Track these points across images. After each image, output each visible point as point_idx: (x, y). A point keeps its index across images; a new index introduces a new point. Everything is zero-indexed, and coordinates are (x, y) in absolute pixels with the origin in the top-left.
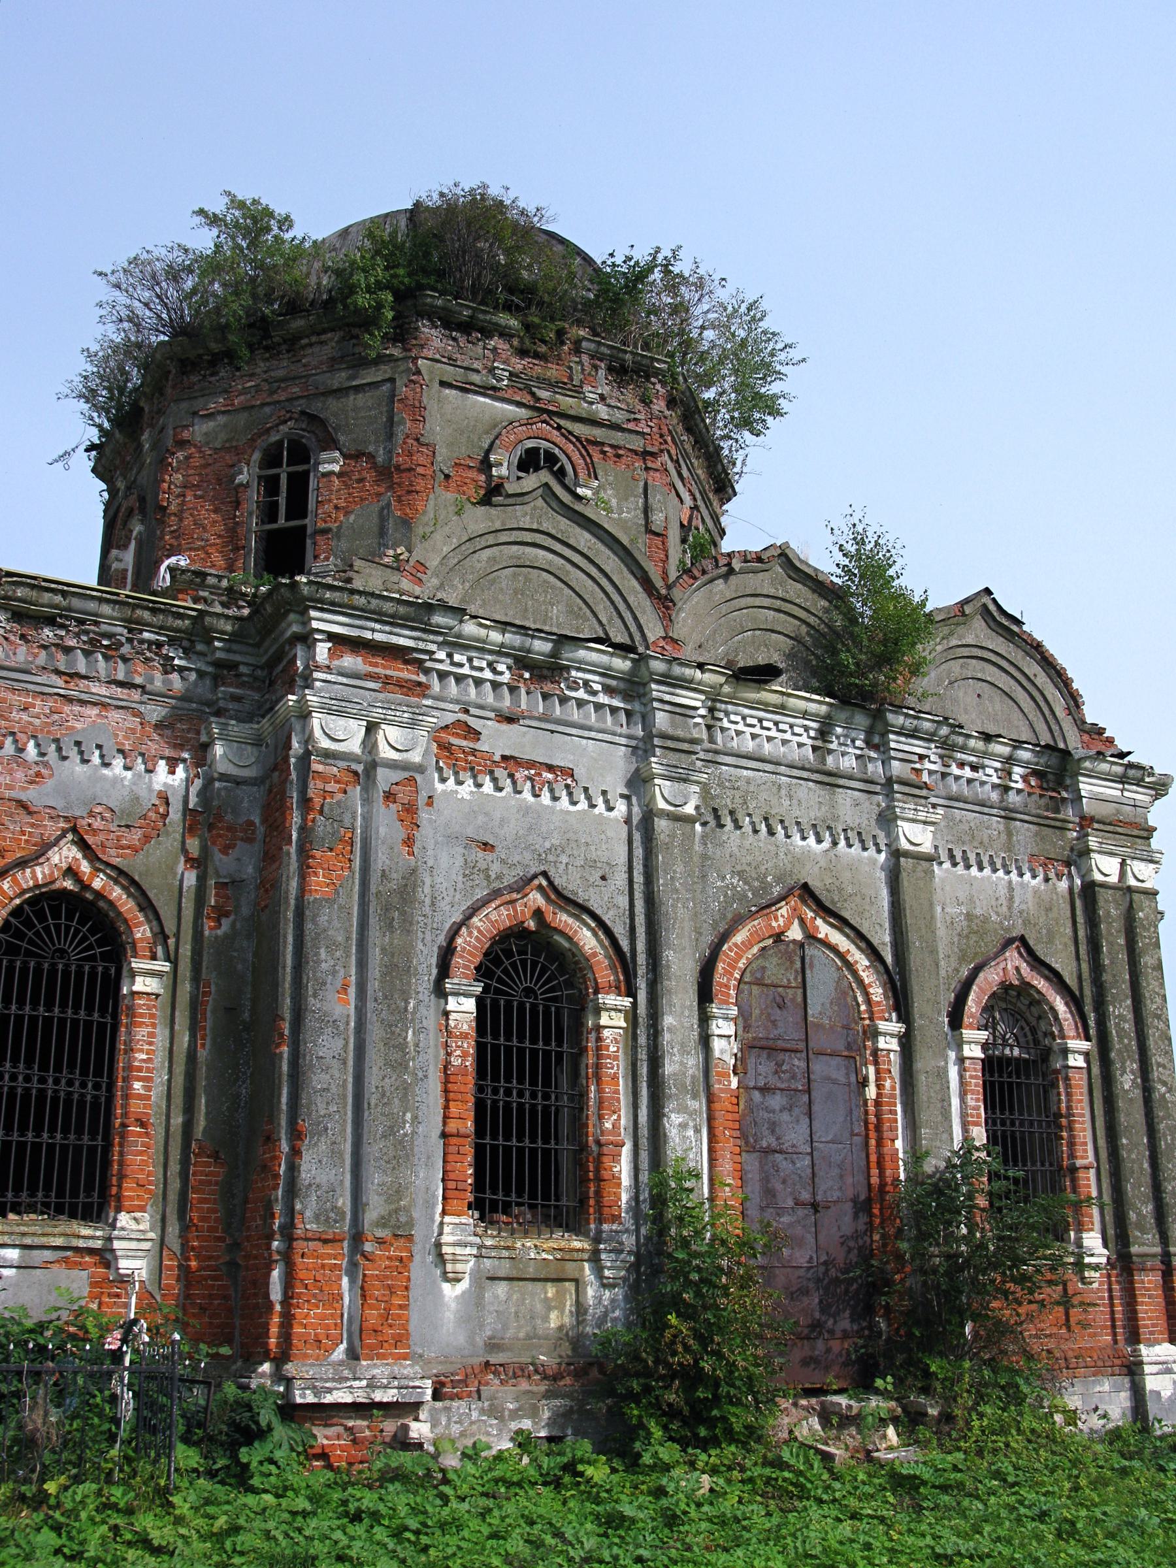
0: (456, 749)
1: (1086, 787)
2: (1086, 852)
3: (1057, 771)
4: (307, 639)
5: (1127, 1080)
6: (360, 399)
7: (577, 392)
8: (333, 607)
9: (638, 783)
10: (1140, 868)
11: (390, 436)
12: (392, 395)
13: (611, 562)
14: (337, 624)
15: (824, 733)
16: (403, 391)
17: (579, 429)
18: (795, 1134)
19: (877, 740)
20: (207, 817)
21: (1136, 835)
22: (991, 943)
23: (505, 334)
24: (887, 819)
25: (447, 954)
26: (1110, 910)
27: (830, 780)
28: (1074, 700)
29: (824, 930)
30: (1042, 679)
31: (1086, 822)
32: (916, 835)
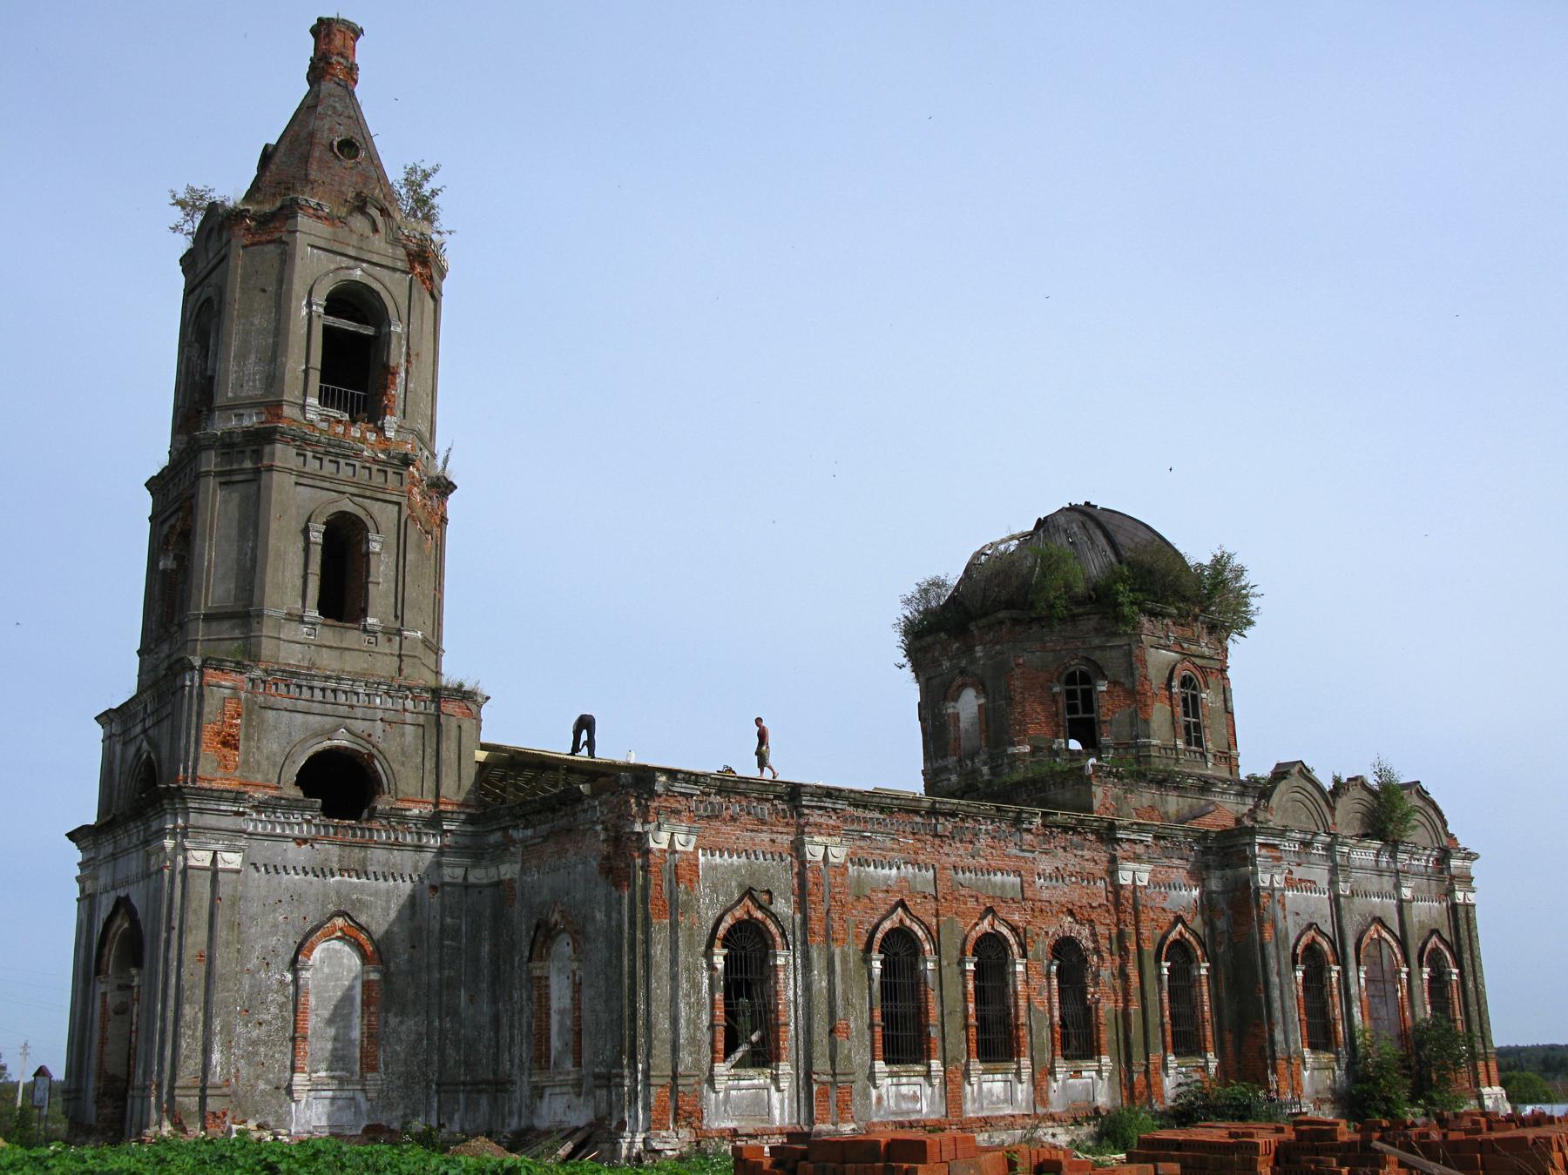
0: (1290, 883)
1: (1453, 863)
2: (1454, 891)
3: (1445, 855)
4: (1252, 845)
5: (1470, 984)
6: (1114, 653)
7: (1197, 643)
8: (1260, 834)
9: (1333, 883)
10: (1470, 895)
11: (1132, 674)
12: (1130, 652)
13: (1317, 795)
14: (1260, 839)
15: (1378, 855)
16: (1137, 652)
17: (1198, 661)
18: (1383, 1013)
19: (1393, 856)
20: (1207, 905)
21: (1467, 880)
22: (1426, 933)
23: (1170, 616)
24: (1397, 886)
25: (1294, 954)
26: (1462, 914)
27: (1380, 873)
28: (1445, 823)
29: (1385, 934)
30: (1434, 816)
31: (1452, 877)
32: (1406, 893)
